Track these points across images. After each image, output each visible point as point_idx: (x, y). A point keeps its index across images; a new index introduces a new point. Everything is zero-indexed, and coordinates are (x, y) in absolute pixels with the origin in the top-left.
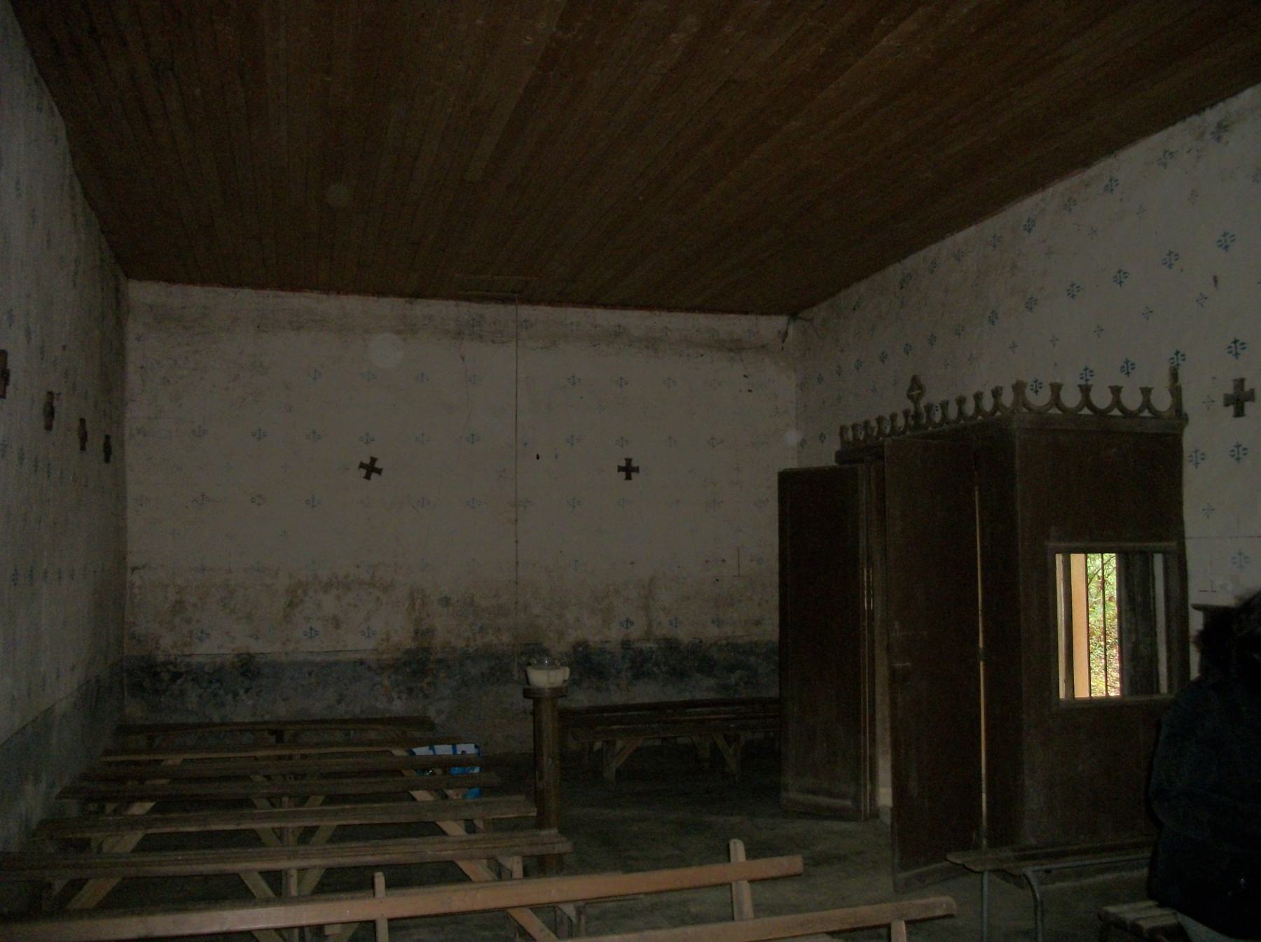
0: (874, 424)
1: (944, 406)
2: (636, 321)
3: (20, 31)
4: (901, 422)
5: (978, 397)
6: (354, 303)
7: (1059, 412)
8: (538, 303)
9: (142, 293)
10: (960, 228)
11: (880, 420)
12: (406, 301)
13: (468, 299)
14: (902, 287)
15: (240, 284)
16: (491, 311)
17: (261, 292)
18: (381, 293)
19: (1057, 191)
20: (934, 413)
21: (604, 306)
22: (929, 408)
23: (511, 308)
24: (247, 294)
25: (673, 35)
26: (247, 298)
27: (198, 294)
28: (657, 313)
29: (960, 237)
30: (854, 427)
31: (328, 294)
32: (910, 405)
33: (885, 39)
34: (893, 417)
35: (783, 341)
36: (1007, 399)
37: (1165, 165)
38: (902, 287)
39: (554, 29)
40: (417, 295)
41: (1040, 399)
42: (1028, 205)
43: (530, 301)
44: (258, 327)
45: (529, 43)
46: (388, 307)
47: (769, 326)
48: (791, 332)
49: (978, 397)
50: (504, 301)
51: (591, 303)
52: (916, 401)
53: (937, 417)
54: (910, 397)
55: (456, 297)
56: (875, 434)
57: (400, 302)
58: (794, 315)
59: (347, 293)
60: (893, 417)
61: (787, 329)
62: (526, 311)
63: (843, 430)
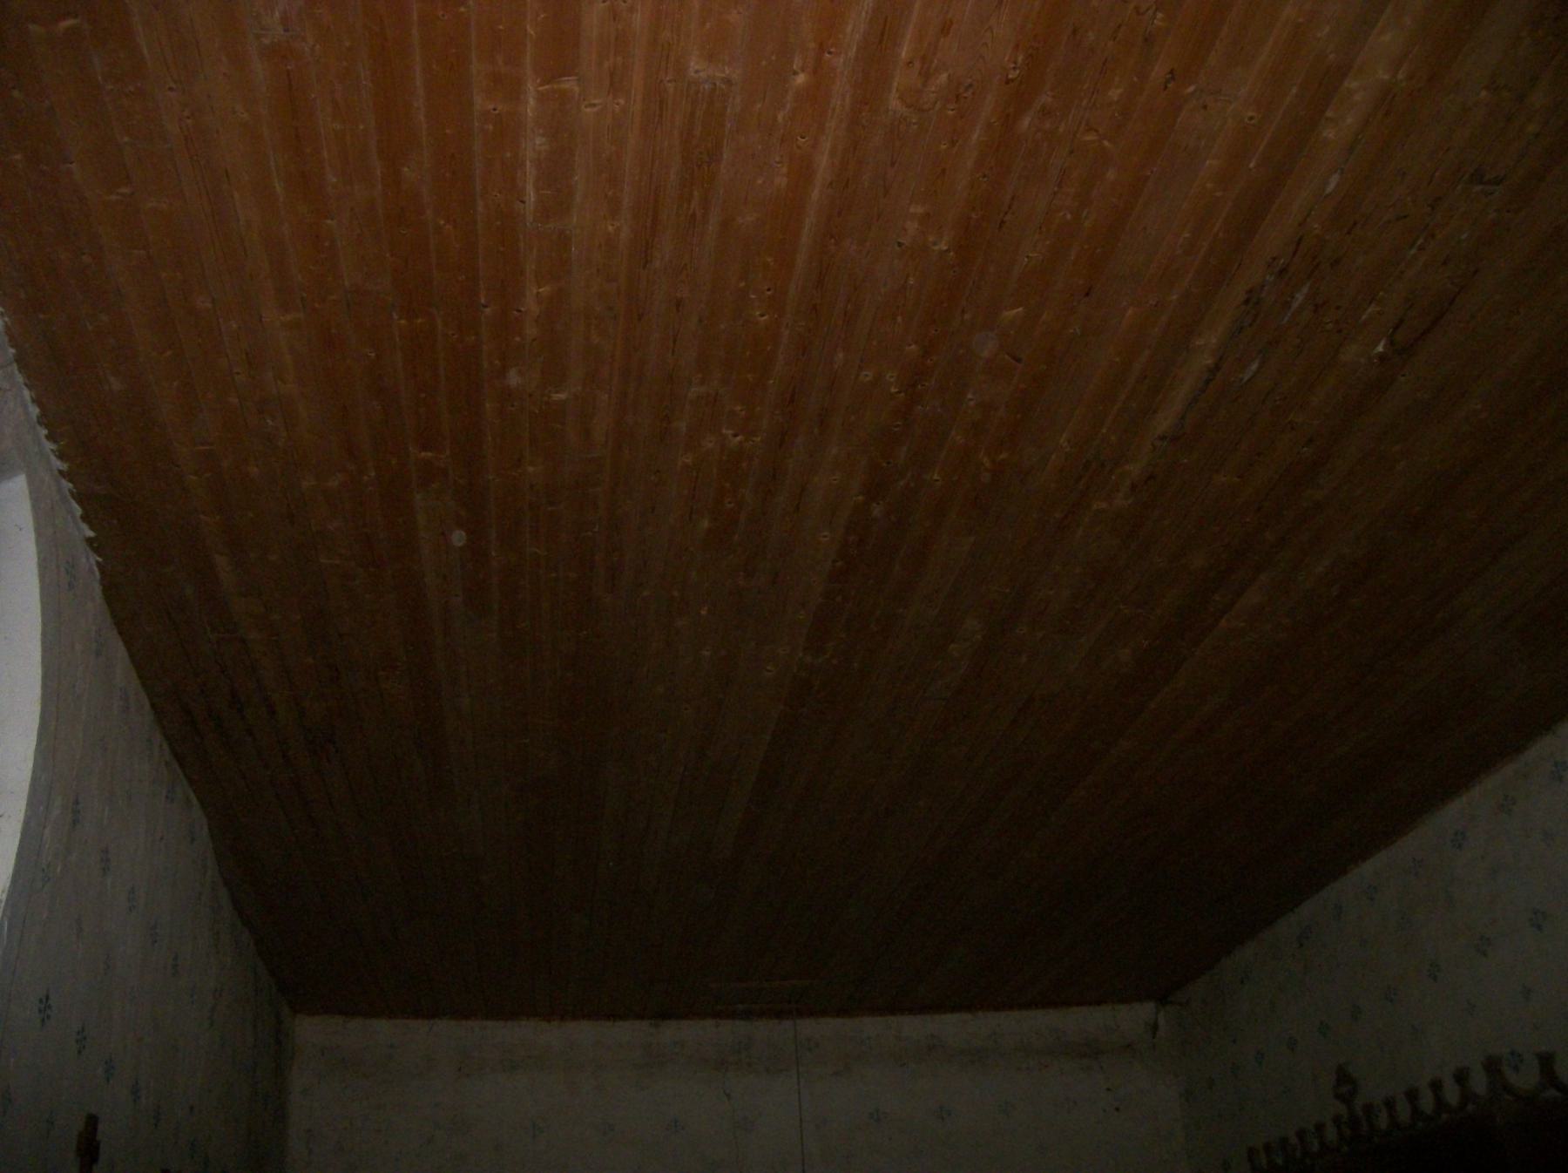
0: (1294, 1140)
1: (1390, 1104)
2: (952, 1027)
3: (147, 706)
4: (1331, 1134)
5: (1436, 1086)
6: (585, 1032)
7: (1558, 1094)
8: (824, 1013)
9: (310, 1031)
10: (1363, 856)
11: (1301, 1134)
12: (651, 1024)
13: (733, 1016)
14: (1301, 945)
15: (433, 1014)
16: (763, 1030)
17: (464, 1022)
18: (613, 1016)
19: (1491, 785)
20: (1377, 1116)
21: (911, 1011)
22: (1368, 1108)
23: (787, 1024)
24: (443, 1026)
25: (952, 646)
26: (447, 1034)
27: (384, 1029)
28: (980, 1013)
29: (1368, 869)
30: (1267, 1148)
31: (549, 1021)
32: (1342, 1109)
33: (1223, 621)
34: (1320, 1127)
35: (1154, 1038)
36: (1479, 1083)
37: (1485, 954)
38: (1301, 945)
39: (801, 655)
40: (664, 1015)
41: (1526, 1079)
42: (1452, 813)
43: (812, 1013)
44: (460, 1069)
45: (770, 674)
46: (626, 1033)
47: (1132, 1018)
48: (1161, 1022)
49: (1436, 1086)
50: (779, 1015)
51: (894, 1008)
52: (1347, 1099)
53: (1383, 1121)
54: (1337, 1096)
55: (717, 1015)
56: (1298, 1154)
57: (644, 1025)
58: (1162, 999)
59: (575, 1017)
60: (1320, 1127)
61: (1157, 1019)
62: (810, 1028)
63: (1251, 1152)
